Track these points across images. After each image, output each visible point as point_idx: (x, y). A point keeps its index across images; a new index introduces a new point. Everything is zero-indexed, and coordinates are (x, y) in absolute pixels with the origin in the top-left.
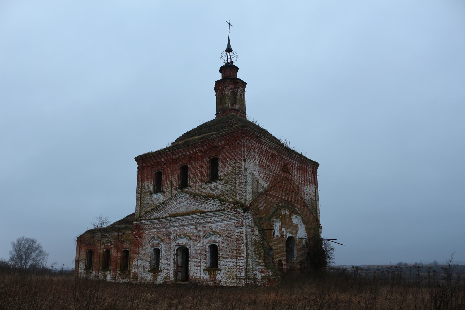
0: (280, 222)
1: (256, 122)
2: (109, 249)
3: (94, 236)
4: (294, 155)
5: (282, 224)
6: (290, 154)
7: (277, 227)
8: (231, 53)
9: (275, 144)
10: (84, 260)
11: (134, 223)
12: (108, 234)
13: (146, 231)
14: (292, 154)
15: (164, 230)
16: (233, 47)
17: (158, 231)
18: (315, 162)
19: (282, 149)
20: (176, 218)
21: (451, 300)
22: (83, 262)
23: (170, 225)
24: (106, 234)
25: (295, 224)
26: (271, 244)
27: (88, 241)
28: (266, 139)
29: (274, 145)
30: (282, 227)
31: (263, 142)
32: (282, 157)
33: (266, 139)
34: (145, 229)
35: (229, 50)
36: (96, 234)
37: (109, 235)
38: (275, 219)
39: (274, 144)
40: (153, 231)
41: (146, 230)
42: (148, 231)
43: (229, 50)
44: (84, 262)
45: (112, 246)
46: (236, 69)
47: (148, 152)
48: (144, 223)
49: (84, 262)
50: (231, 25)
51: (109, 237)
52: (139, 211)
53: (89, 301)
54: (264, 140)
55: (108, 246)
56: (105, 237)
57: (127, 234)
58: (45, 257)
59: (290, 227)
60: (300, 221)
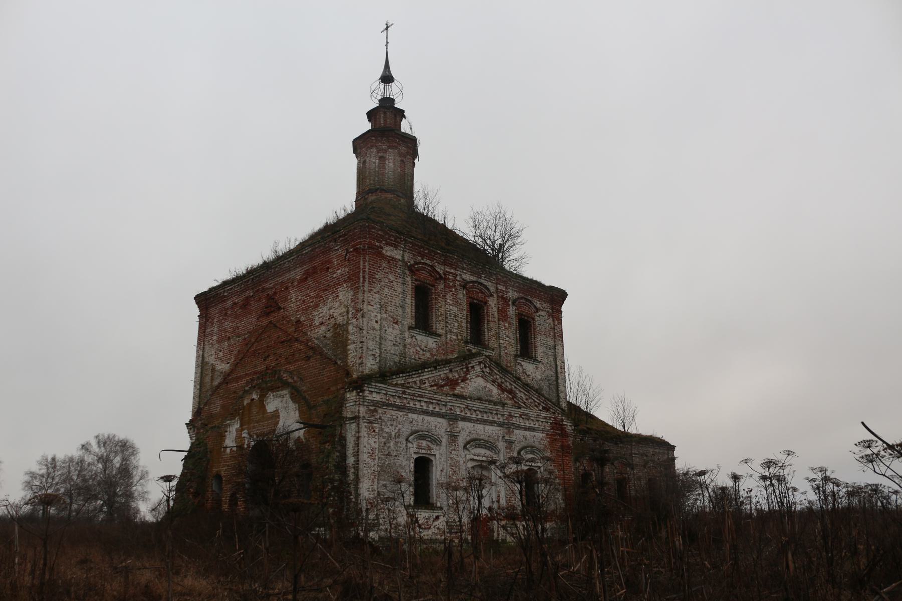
0: (237, 423)
4: (285, 263)
5: (241, 425)
6: (276, 270)
7: (233, 433)
9: (242, 281)
14: (280, 265)
18: (197, 303)
19: (256, 277)
23: (415, 406)
25: (271, 412)
26: (219, 468)
28: (226, 289)
29: (241, 284)
30: (242, 430)
31: (224, 297)
32: (263, 289)
33: (226, 288)
35: (387, 78)
38: (229, 422)
39: (240, 283)
43: (387, 78)
47: (193, 384)
50: (387, 32)
54: (224, 292)
58: (505, 444)
59: (259, 423)
60: (284, 401)
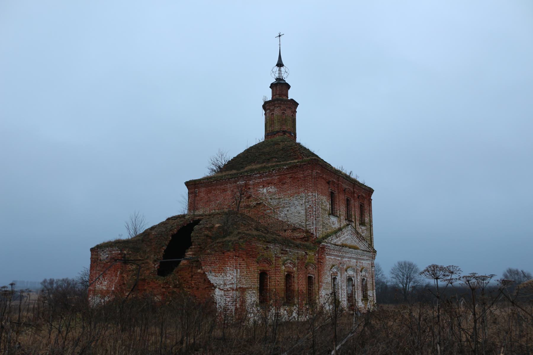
1: (350, 174)
2: (290, 272)
3: (267, 248)
8: (282, 68)
10: (254, 288)
11: (322, 243)
12: (288, 250)
13: (327, 257)
15: (340, 259)
16: (284, 62)
17: (335, 259)
20: (350, 249)
21: (477, 316)
22: (254, 293)
24: (286, 249)
27: (259, 253)
34: (326, 254)
36: (272, 245)
37: (290, 252)
40: (332, 258)
41: (327, 256)
42: (328, 257)
44: (254, 291)
45: (295, 269)
46: (288, 86)
48: (329, 246)
49: (254, 291)
50: (280, 38)
51: (290, 255)
52: (239, 209)
53: (463, 334)
55: (290, 267)
56: (286, 254)
57: (310, 255)
